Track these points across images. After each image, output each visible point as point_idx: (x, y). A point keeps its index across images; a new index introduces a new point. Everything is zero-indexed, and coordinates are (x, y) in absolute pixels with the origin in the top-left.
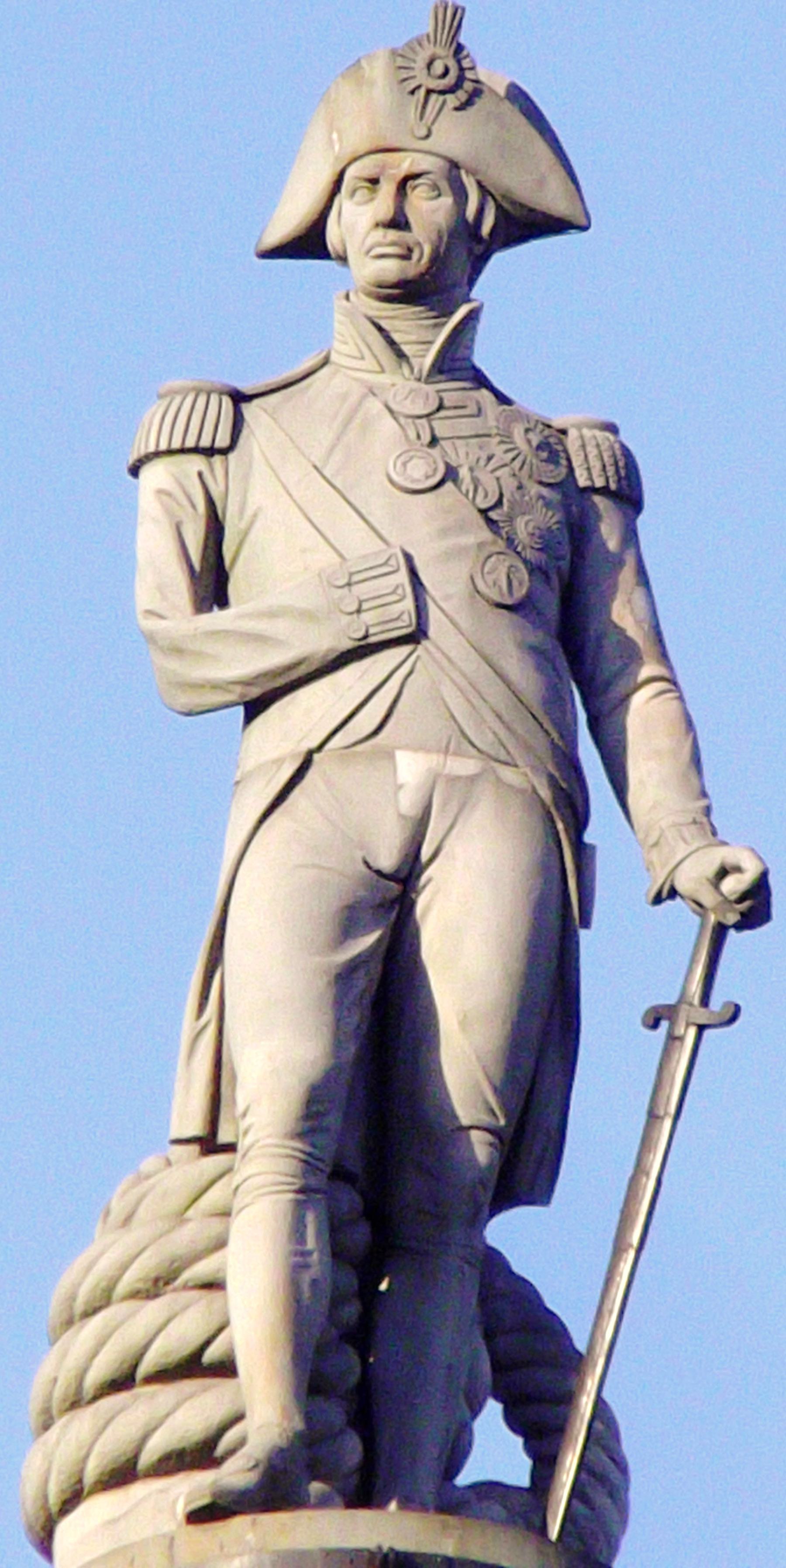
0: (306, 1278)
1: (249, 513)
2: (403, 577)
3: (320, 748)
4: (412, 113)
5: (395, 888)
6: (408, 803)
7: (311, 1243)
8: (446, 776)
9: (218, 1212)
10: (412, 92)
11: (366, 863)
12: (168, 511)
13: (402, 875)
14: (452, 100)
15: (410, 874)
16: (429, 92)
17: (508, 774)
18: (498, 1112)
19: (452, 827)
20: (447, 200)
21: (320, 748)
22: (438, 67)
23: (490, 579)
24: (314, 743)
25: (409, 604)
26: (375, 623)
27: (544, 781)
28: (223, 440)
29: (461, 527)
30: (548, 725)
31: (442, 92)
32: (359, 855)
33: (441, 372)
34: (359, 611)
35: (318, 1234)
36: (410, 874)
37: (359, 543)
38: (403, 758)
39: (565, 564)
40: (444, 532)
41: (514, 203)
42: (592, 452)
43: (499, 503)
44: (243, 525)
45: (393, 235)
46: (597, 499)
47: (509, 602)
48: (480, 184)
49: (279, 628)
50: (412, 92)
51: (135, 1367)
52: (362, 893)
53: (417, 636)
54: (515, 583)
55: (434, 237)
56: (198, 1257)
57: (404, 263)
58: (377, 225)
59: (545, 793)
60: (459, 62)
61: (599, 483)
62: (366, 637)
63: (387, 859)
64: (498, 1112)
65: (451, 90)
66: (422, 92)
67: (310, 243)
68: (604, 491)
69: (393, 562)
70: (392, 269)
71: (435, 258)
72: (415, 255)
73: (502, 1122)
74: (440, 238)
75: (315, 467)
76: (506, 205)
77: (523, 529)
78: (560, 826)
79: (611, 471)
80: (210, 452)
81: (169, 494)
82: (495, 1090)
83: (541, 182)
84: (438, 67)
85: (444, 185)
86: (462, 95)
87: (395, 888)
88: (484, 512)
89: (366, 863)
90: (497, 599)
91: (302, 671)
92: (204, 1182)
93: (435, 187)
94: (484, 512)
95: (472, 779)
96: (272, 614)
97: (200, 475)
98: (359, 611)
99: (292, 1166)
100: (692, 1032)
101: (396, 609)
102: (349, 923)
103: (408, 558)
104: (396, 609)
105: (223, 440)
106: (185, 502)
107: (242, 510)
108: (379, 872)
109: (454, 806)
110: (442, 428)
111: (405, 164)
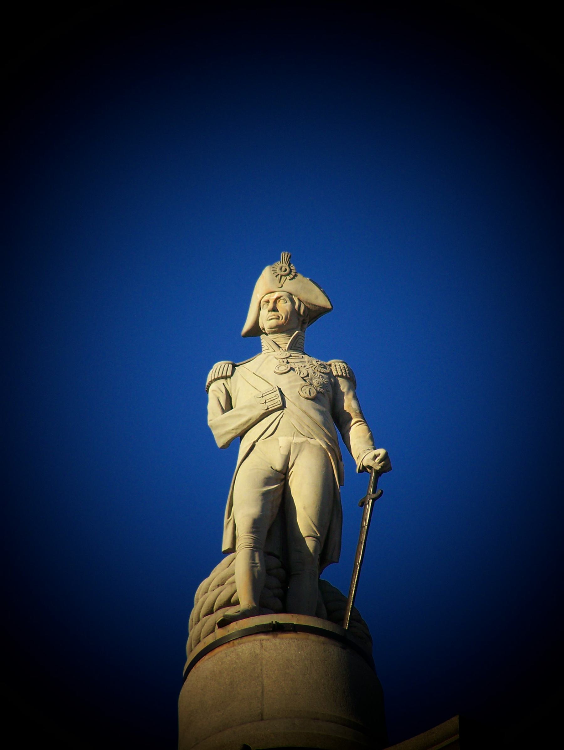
0: (256, 570)
1: (237, 390)
2: (278, 392)
3: (257, 441)
4: (277, 282)
5: (283, 476)
6: (284, 452)
7: (257, 561)
8: (295, 443)
10: (276, 276)
11: (271, 467)
12: (215, 395)
14: (288, 277)
15: (286, 472)
16: (281, 276)
17: (312, 441)
18: (317, 532)
19: (297, 457)
20: (289, 303)
21: (257, 441)
22: (283, 269)
23: (304, 392)
24: (255, 440)
25: (280, 399)
26: (270, 406)
27: (324, 442)
29: (296, 381)
30: (324, 429)
31: (286, 275)
32: (270, 466)
33: (291, 349)
34: (265, 403)
35: (260, 559)
36: (286, 472)
37: (264, 387)
38: (280, 439)
39: (331, 393)
40: (290, 382)
41: (309, 304)
42: (338, 367)
43: (308, 376)
44: (236, 394)
45: (273, 313)
46: (339, 379)
47: (309, 397)
48: (299, 300)
49: (244, 412)
50: (276, 276)
51: (213, 607)
52: (271, 475)
53: (283, 407)
54: (311, 392)
55: (286, 313)
56: (230, 577)
57: (278, 320)
58: (269, 311)
59: (324, 446)
60: (290, 268)
61: (340, 374)
62: (268, 409)
63: (278, 466)
64: (317, 532)
65: (288, 274)
66: (280, 276)
67: (256, 331)
68: (342, 376)
69: (275, 389)
70: (274, 322)
71: (286, 318)
72: (281, 319)
73: (319, 535)
74: (288, 313)
76: (308, 305)
77: (315, 382)
78: (330, 454)
79: (343, 371)
80: (226, 378)
81: (215, 391)
82: (315, 526)
83: (317, 298)
84: (283, 269)
85: (287, 299)
86: (292, 276)
87: (283, 476)
88: (302, 378)
89: (271, 467)
90: (306, 396)
91: (251, 422)
92: (231, 560)
93: (285, 300)
94: (302, 378)
95: (302, 444)
96: (242, 409)
97: (224, 384)
98: (265, 403)
99: (250, 541)
100: (371, 501)
101: (276, 401)
102: (268, 481)
103: (280, 389)
104: (276, 401)
105: (229, 373)
106: (220, 392)
107: (235, 390)
108: (276, 470)
109: (297, 451)
110: (289, 360)
111: (276, 295)
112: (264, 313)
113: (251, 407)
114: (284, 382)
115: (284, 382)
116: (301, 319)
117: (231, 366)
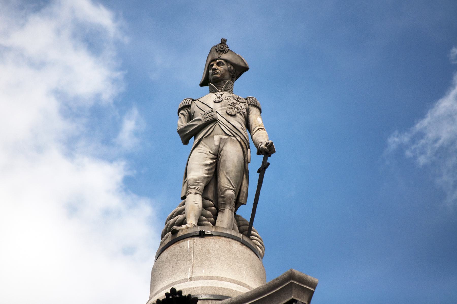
5: (216, 157)
6: (217, 143)
9: (250, 116)
13: (216, 154)
22: (222, 47)
28: (190, 104)
37: (208, 109)
39: (246, 113)
63: (214, 148)
75: (203, 103)
111: (218, 61)
112: (211, 71)
113: (199, 120)
114: (218, 107)
115: (218, 107)
116: (231, 75)
117: (191, 100)
